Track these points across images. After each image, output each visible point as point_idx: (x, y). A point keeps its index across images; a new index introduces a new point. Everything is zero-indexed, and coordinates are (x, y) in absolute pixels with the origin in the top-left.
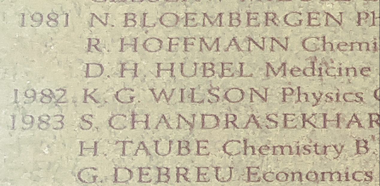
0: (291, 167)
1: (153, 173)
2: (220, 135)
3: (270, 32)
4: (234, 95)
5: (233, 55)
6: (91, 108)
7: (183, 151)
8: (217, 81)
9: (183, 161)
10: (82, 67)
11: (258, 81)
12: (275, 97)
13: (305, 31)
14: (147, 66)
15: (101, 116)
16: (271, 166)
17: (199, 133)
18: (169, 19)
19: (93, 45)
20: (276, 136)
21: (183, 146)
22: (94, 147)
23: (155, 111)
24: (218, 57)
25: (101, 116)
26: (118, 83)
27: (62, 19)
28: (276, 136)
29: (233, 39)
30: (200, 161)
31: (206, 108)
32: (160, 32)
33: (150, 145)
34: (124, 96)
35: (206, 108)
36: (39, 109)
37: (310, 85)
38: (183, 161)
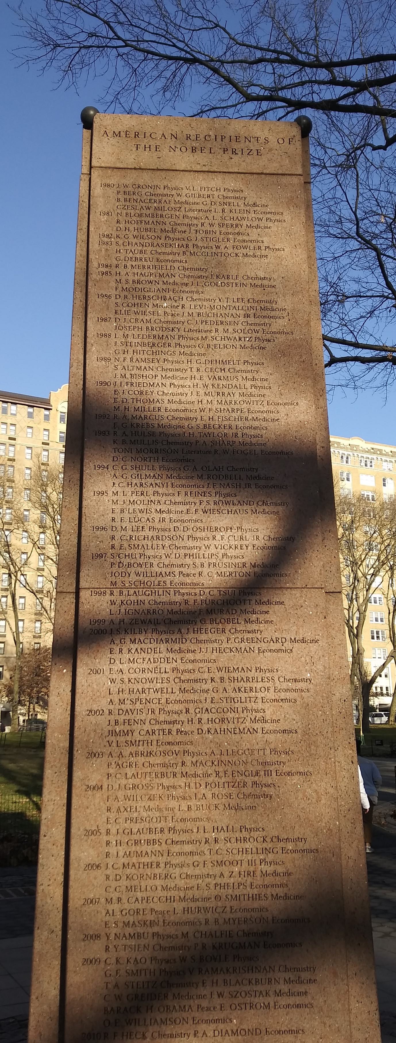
0: (167, 258)
1: (134, 258)
2: (150, 248)
3: (162, 220)
4: (153, 237)
5: (152, 226)
6: (118, 240)
7: (194, 151)
8: (149, 233)
9: (141, 256)
10: (115, 228)
11: (159, 234)
12: (163, 238)
13: (170, 220)
14: (132, 229)
15: (121, 242)
16: (162, 258)
17: (145, 248)
18: (137, 215)
19: (118, 222)
20: (163, 249)
21: (141, 252)
22: (377, 64)
23: (135, 241)
24: (148, 226)
25: (121, 242)
26: (124, 233)
27: (110, 214)
28: (163, 249)
29: (324, 339)
30: (146, 256)
31: (146, 241)
32: (134, 218)
33: (133, 250)
34: (205, 203)
35: (146, 241)
36: (106, 240)
37: (171, 235)
38: (141, 256)
